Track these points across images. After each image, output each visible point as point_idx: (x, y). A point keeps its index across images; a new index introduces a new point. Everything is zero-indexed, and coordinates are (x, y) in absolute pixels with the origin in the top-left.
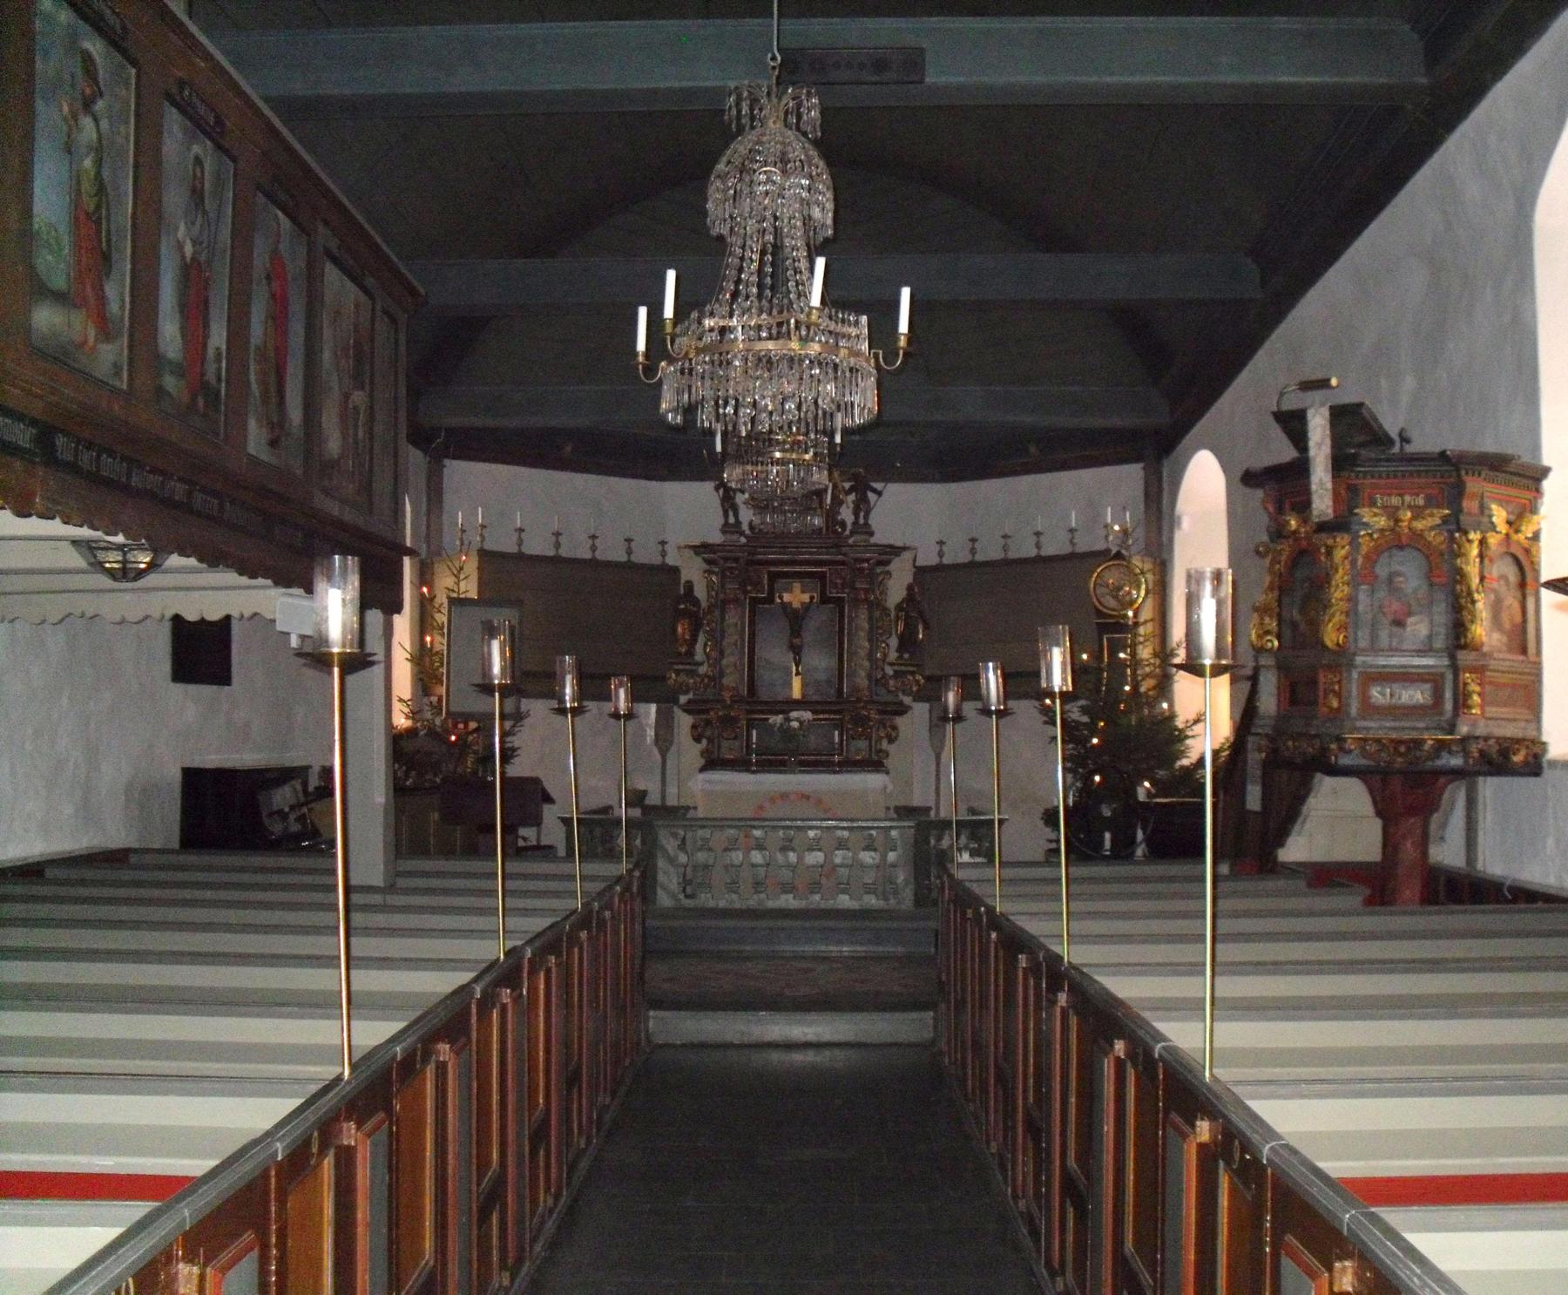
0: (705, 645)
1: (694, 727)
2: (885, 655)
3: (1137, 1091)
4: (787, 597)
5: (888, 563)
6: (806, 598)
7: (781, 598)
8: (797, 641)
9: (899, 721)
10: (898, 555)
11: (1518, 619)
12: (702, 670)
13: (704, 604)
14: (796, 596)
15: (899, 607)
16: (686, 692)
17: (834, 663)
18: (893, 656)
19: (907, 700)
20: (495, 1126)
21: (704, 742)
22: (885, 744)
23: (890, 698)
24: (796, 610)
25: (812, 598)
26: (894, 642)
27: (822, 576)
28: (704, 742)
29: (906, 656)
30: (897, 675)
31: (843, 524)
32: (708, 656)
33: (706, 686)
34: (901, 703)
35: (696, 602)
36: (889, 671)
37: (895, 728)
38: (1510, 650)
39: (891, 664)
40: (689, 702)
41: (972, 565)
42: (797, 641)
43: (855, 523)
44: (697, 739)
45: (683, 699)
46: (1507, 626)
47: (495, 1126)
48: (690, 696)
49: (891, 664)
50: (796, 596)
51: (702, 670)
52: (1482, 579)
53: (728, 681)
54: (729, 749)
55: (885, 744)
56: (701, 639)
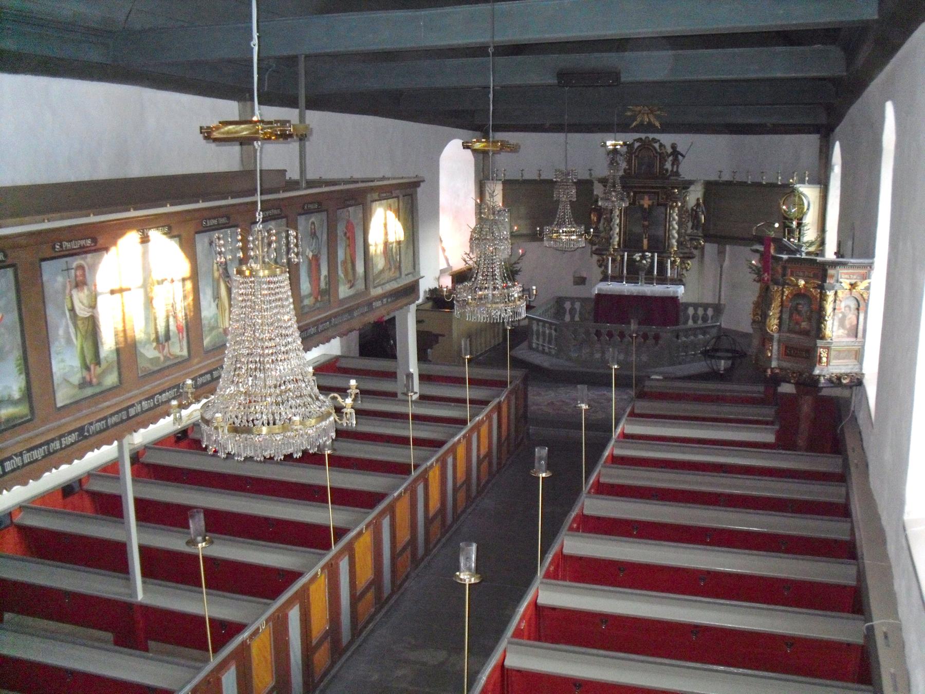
11: (855, 322)
31: (667, 170)
34: (691, 253)
38: (848, 335)
43: (672, 171)
46: (848, 326)
52: (834, 309)
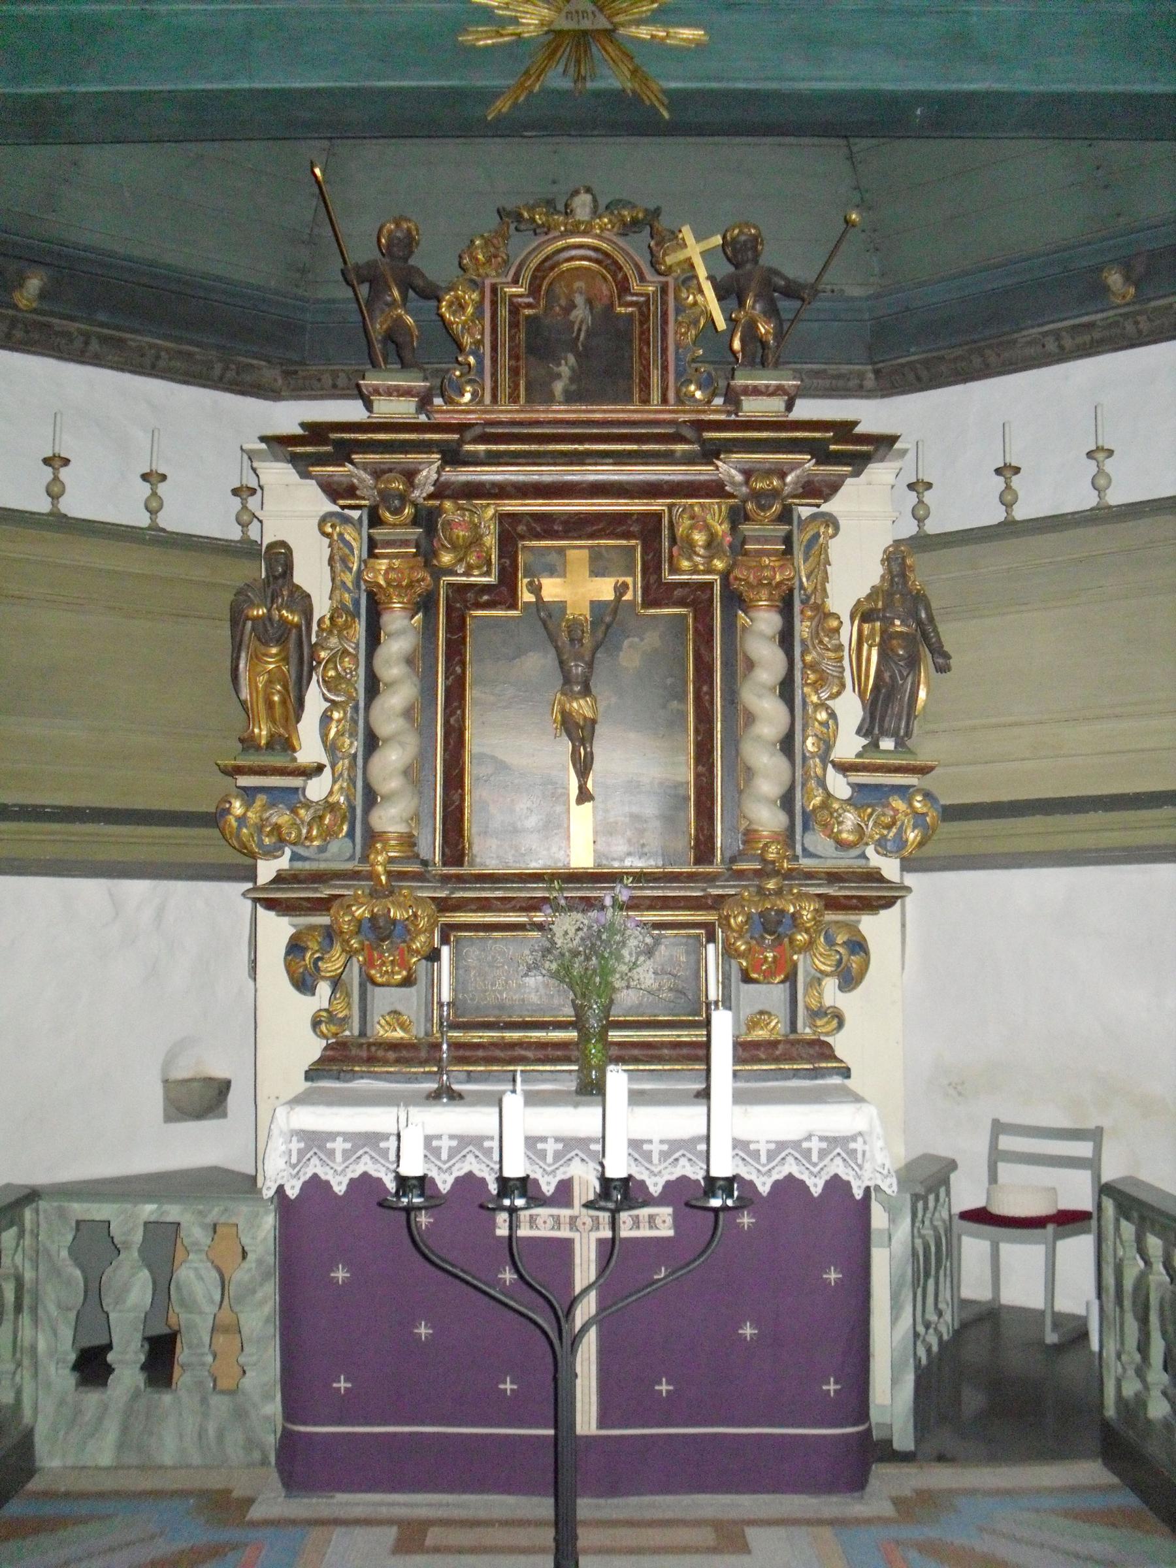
0: (326, 719)
1: (295, 947)
2: (827, 745)
3: (616, 1437)
4: (552, 589)
5: (830, 489)
6: (604, 589)
7: (536, 590)
8: (581, 707)
9: (871, 925)
10: (859, 462)
12: (317, 789)
13: (322, 607)
14: (576, 586)
15: (864, 614)
16: (272, 853)
17: (687, 773)
18: (849, 745)
19: (890, 868)
20: (413, 436)
21: (324, 989)
22: (831, 993)
23: (844, 862)
24: (574, 626)
25: (621, 589)
26: (850, 709)
27: (649, 529)
28: (324, 989)
29: (887, 744)
30: (864, 796)
32: (331, 748)
33: (329, 834)
34: (875, 877)
35: (303, 602)
36: (839, 785)
37: (859, 946)
39: (844, 768)
40: (280, 879)
41: (1009, 529)
42: (581, 707)
44: (303, 984)
45: (267, 870)
47: (413, 436)
48: (283, 862)
49: (844, 768)
50: (576, 586)
51: (317, 789)
53: (390, 819)
54: (396, 1013)
55: (831, 993)
56: (315, 700)
